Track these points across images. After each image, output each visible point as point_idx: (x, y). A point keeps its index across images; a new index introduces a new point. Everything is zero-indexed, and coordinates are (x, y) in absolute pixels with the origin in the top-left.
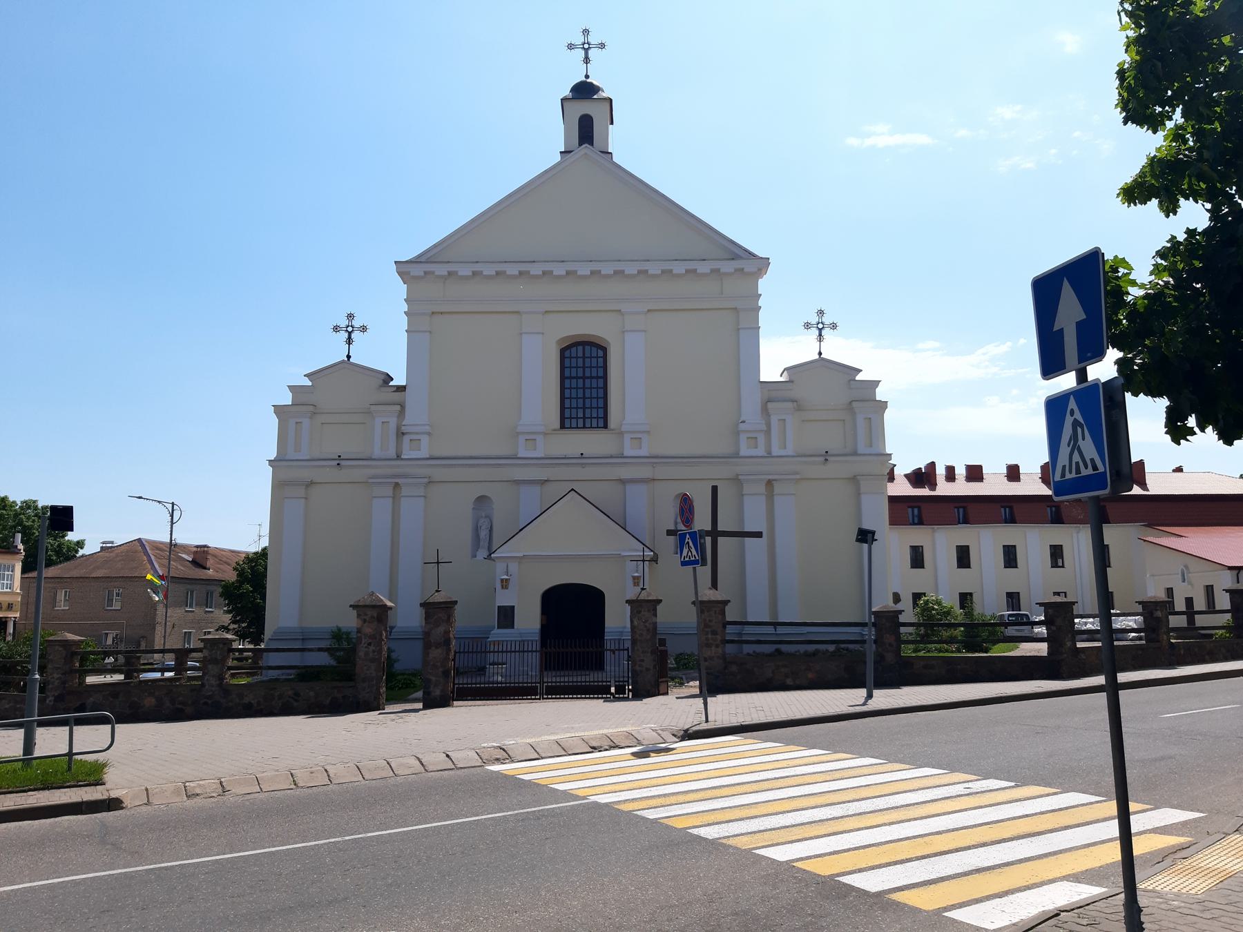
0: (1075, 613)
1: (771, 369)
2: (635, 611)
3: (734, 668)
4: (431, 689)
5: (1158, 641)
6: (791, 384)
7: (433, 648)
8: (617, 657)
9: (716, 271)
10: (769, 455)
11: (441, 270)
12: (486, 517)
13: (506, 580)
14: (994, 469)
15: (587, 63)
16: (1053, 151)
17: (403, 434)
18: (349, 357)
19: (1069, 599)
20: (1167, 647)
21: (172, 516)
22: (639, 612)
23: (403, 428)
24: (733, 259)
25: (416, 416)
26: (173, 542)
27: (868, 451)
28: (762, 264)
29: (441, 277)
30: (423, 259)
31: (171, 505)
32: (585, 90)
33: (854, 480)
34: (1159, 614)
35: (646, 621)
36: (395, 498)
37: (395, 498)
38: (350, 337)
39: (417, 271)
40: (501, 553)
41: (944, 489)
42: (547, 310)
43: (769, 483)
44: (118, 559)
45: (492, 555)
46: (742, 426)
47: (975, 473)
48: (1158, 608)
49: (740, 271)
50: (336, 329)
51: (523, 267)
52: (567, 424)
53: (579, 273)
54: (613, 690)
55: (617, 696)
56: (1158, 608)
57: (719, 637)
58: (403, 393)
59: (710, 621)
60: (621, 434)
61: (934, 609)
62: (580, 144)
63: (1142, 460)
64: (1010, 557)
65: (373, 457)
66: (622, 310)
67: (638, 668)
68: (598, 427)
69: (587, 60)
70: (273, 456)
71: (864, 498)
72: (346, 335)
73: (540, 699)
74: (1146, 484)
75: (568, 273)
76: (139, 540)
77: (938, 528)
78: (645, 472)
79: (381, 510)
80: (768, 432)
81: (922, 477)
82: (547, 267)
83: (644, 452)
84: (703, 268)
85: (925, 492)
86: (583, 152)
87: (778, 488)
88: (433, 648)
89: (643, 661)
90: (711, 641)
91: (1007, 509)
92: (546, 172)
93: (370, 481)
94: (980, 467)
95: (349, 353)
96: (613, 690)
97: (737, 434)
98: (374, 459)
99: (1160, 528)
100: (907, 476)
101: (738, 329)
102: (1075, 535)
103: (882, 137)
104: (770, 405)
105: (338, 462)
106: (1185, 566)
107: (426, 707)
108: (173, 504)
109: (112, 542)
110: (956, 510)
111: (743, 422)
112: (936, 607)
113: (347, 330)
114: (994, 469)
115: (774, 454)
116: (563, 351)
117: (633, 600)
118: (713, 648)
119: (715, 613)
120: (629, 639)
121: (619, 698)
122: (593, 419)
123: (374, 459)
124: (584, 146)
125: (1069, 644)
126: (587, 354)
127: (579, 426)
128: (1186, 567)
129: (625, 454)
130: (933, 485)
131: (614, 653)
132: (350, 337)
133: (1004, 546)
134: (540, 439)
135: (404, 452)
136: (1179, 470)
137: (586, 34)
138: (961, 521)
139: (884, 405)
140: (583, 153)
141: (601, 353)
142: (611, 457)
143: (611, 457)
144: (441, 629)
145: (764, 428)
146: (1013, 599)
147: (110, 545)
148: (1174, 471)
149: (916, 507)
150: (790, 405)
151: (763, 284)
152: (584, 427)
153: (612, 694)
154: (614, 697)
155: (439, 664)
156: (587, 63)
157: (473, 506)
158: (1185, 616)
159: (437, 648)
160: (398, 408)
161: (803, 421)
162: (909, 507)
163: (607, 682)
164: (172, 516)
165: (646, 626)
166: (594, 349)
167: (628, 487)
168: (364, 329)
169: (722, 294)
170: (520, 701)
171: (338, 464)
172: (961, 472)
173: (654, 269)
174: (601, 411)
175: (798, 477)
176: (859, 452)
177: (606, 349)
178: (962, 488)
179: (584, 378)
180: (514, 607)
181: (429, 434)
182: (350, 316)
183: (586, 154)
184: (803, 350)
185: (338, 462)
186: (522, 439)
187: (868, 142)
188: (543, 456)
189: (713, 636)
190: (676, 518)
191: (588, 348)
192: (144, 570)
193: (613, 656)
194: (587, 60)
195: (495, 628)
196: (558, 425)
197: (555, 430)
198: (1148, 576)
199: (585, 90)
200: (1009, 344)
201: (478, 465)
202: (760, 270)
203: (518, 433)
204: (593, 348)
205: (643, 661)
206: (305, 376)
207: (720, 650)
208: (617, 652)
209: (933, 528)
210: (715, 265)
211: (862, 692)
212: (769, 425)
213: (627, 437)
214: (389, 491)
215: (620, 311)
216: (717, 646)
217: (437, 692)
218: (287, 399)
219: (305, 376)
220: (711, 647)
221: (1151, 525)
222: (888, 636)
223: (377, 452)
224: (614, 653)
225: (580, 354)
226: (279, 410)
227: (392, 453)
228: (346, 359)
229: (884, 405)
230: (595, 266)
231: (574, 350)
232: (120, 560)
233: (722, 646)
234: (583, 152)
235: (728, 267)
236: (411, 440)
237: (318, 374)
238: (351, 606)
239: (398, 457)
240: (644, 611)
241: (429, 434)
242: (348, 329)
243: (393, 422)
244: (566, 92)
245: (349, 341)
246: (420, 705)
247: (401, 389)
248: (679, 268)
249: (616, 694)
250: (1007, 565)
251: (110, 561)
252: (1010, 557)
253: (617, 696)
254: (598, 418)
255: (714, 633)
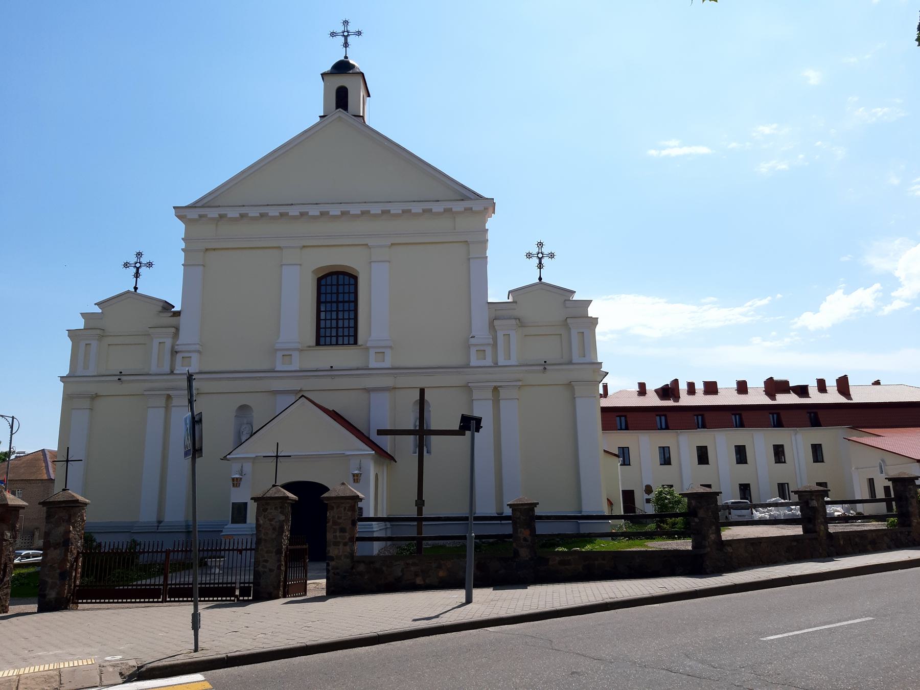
0: (718, 504)
1: (497, 293)
2: (261, 509)
3: (362, 568)
4: (47, 592)
5: (815, 532)
6: (515, 304)
7: (52, 549)
8: (244, 557)
9: (448, 211)
10: (496, 365)
11: (213, 213)
12: (247, 424)
13: (237, 479)
14: (727, 385)
15: (346, 47)
16: (801, 156)
17: (177, 352)
18: (136, 288)
19: (713, 490)
20: (825, 538)
21: (12, 427)
22: (265, 510)
23: (176, 347)
24: (463, 200)
25: (187, 337)
26: (12, 449)
27: (582, 360)
28: (488, 206)
29: (213, 219)
30: (200, 204)
31: (11, 418)
32: (343, 67)
33: (570, 386)
34: (814, 503)
35: (271, 520)
36: (167, 408)
37: (167, 408)
38: (540, 263)
39: (193, 214)
40: (236, 454)
41: (686, 400)
42: (305, 245)
43: (496, 389)
44: (23, 465)
45: (227, 457)
46: (472, 341)
47: (711, 388)
48: (813, 498)
49: (469, 210)
50: (126, 265)
51: (283, 209)
52: (322, 342)
53: (331, 213)
54: (237, 593)
55: (241, 598)
56: (813, 498)
57: (347, 535)
58: (178, 317)
59: (339, 518)
60: (367, 348)
61: (666, 499)
62: (337, 109)
63: (879, 380)
64: (741, 454)
65: (150, 373)
66: (369, 244)
67: (261, 569)
68: (349, 344)
69: (346, 45)
70: (66, 372)
71: (578, 401)
72: (537, 261)
73: (162, 602)
74: (850, 395)
75: (322, 214)
76: (43, 451)
77: (680, 432)
78: (388, 382)
79: (155, 417)
80: (495, 345)
81: (669, 391)
82: (304, 209)
83: (387, 364)
84: (437, 208)
85: (670, 403)
86: (337, 115)
87: (503, 393)
88: (52, 549)
89: (266, 561)
90: (339, 540)
91: (737, 416)
92: (305, 132)
93: (145, 393)
94: (715, 384)
95: (136, 285)
96: (237, 593)
97: (468, 347)
98: (151, 375)
99: (862, 430)
100: (656, 391)
101: (469, 259)
102: (793, 438)
103: (675, 149)
104: (496, 323)
105: (119, 377)
106: (882, 460)
107: (41, 610)
108: (13, 418)
109: (24, 453)
110: (695, 417)
111: (473, 337)
112: (668, 497)
113: (135, 266)
114: (727, 385)
115: (499, 364)
116: (319, 280)
117: (258, 498)
118: (341, 546)
119: (345, 509)
120: (415, 525)
121: (244, 600)
122: (345, 337)
123: (151, 375)
124: (338, 110)
125: (713, 537)
126: (341, 282)
127: (345, 343)
128: (883, 461)
129: (371, 366)
130: (677, 397)
131: (241, 553)
132: (540, 263)
133: (735, 446)
134: (296, 354)
135: (177, 368)
136: (877, 383)
137: (346, 24)
138: (700, 427)
139: (595, 321)
140: (338, 116)
141: (352, 281)
142: (357, 369)
143: (357, 369)
144: (61, 529)
145: (491, 341)
146: (745, 489)
147: (23, 455)
148: (873, 384)
149: (663, 415)
150: (513, 322)
151: (491, 224)
152: (337, 344)
153: (236, 596)
154: (238, 600)
155: (56, 565)
156: (346, 47)
157: (235, 415)
158: (885, 503)
159: (55, 549)
160: (173, 330)
161: (525, 336)
162: (657, 415)
163: (231, 583)
164: (12, 427)
165: (271, 525)
166: (347, 278)
167: (373, 395)
168: (150, 265)
169: (455, 229)
170: (143, 605)
171: (119, 379)
172: (699, 387)
173: (396, 209)
174: (352, 330)
175: (520, 383)
176: (573, 362)
177: (357, 277)
178: (701, 400)
179: (337, 302)
180: (246, 503)
181: (199, 352)
182: (139, 255)
183: (340, 117)
184: (528, 276)
185: (119, 377)
186: (279, 354)
187: (664, 153)
188: (298, 369)
189: (342, 534)
190: (416, 422)
191: (341, 277)
192: (41, 474)
193: (239, 556)
194: (346, 45)
195: (229, 522)
196: (313, 342)
197: (309, 347)
198: (853, 469)
199: (343, 67)
200: (769, 298)
201: (220, 378)
202: (486, 209)
203: (277, 350)
204: (346, 277)
205: (266, 561)
206: (95, 304)
207: (348, 549)
208: (244, 552)
209: (677, 432)
210: (448, 205)
211: (459, 595)
212: (495, 339)
213: (372, 352)
214: (162, 402)
215: (367, 245)
216: (345, 544)
217: (52, 595)
218: (80, 324)
219: (95, 304)
220: (339, 546)
221: (855, 427)
222: (523, 530)
223: (154, 369)
224: (241, 553)
225: (335, 282)
226: (72, 334)
227: (167, 369)
228: (134, 290)
229: (595, 321)
230: (345, 208)
231: (329, 278)
232: (24, 467)
233: (350, 544)
234: (337, 115)
235: (458, 207)
236: (183, 357)
237: (107, 303)
238: (40, 504)
239: (172, 373)
240: (271, 509)
241: (199, 352)
242: (136, 265)
243: (168, 342)
244: (328, 68)
245: (540, 266)
246: (34, 607)
247: (178, 314)
248: (417, 208)
249: (240, 596)
250: (777, 461)
251: (17, 467)
252: (741, 454)
253: (241, 598)
254: (349, 336)
255: (343, 530)
